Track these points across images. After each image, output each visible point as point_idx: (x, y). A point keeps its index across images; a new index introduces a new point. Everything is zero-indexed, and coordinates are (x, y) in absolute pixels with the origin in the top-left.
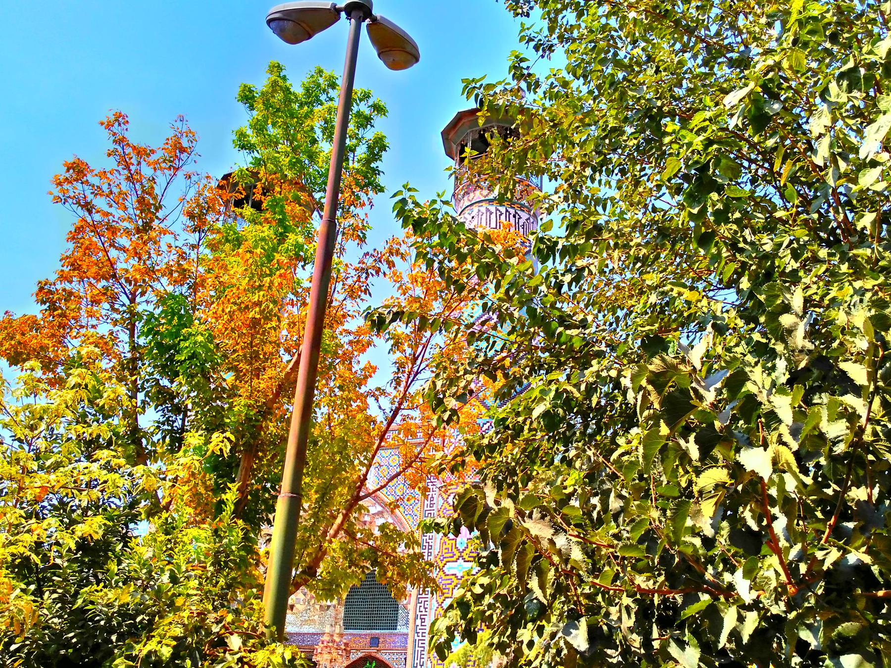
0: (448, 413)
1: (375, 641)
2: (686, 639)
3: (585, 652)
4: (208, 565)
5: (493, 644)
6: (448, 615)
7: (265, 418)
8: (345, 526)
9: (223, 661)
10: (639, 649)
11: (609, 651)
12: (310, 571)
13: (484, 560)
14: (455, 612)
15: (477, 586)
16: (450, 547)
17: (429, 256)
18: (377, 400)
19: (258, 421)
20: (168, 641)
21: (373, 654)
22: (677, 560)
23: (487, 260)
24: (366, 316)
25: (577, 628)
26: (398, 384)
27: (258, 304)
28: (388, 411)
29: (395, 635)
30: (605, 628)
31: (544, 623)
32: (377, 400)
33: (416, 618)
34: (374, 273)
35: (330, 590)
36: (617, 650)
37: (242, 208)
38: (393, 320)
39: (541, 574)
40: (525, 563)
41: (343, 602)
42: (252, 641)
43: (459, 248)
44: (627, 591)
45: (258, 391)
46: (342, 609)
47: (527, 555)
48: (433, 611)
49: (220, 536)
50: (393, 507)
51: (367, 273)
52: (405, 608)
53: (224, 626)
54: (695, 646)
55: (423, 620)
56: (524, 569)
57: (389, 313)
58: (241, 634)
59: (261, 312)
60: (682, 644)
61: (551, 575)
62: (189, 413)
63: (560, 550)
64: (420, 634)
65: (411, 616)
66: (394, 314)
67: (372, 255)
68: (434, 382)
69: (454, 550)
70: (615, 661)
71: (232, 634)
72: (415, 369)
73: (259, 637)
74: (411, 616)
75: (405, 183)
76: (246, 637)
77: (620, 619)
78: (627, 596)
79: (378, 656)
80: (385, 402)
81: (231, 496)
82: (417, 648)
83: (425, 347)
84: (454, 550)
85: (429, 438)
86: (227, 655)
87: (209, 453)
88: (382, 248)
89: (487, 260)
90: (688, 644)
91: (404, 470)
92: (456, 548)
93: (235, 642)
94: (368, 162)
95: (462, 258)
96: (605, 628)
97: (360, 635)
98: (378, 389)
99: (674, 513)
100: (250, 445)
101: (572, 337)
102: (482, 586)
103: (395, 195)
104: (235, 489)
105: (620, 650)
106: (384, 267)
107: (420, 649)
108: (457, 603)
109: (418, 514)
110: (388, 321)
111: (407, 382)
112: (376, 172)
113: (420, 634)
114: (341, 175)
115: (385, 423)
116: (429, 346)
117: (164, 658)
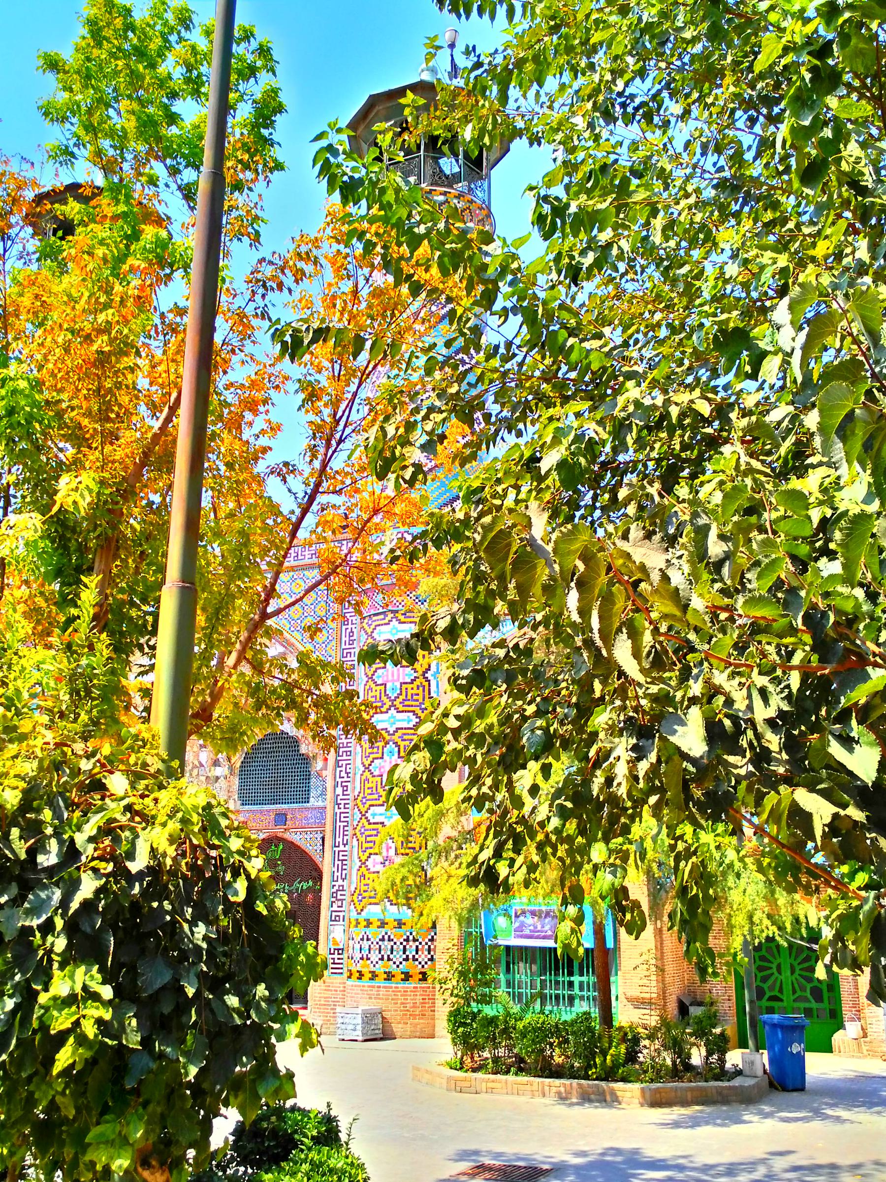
0: (411, 470)
1: (281, 818)
2: (854, 734)
3: (702, 757)
4: (62, 693)
5: (470, 797)
6: (413, 758)
7: (126, 499)
8: (249, 654)
9: (102, 809)
10: (780, 753)
11: (731, 759)
12: (205, 714)
13: (464, 682)
14: (421, 754)
15: (451, 718)
16: (378, 694)
17: (368, 236)
18: (284, 480)
19: (117, 503)
20: (14, 782)
21: (280, 835)
22: (832, 619)
23: (454, 245)
24: (273, 335)
25: (683, 723)
26: (314, 456)
27: (106, 329)
28: (301, 495)
29: (307, 809)
30: (727, 723)
31: (551, 759)
32: (284, 480)
33: (336, 786)
34: (275, 286)
35: (231, 739)
36: (744, 757)
37: (66, 204)
38: (313, 341)
39: (634, 635)
40: (610, 617)
41: (237, 771)
42: (144, 783)
43: (411, 228)
44: (759, 666)
45: (113, 462)
46: (236, 781)
47: (614, 604)
48: (358, 777)
49: (76, 652)
50: (313, 631)
51: (264, 286)
52: (319, 775)
53: (99, 761)
54: (870, 744)
55: (345, 788)
56: (611, 625)
57: (308, 329)
58: (127, 772)
59: (111, 341)
60: (848, 742)
61: (647, 638)
62: (13, 500)
63: (677, 589)
64: (342, 806)
65: (329, 784)
66: (315, 331)
67: (271, 263)
68: (382, 428)
69: (384, 698)
70: (743, 772)
71: (111, 773)
72: (338, 436)
73: (154, 776)
74: (329, 784)
75: (333, 120)
76: (135, 777)
77: (750, 708)
78: (760, 673)
79: (287, 836)
80: (297, 484)
81: (89, 597)
82: (338, 824)
83: (350, 406)
84: (384, 698)
85: (359, 534)
86: (107, 800)
87: (55, 509)
88: (286, 248)
89: (454, 245)
90: (857, 742)
91: (326, 577)
92: (386, 695)
93: (117, 783)
94: (255, 126)
95: (415, 242)
96: (727, 723)
97: (261, 812)
98: (286, 464)
99: (848, 535)
100: (108, 540)
101: (589, 352)
102: (457, 717)
103: (318, 138)
104: (93, 585)
105: (748, 755)
106: (288, 280)
107: (342, 824)
108: (425, 742)
109: (333, 654)
110: (306, 342)
111: (326, 455)
112: (269, 142)
113: (342, 806)
114: (226, 123)
115: (298, 512)
116: (357, 401)
117: (9, 806)
